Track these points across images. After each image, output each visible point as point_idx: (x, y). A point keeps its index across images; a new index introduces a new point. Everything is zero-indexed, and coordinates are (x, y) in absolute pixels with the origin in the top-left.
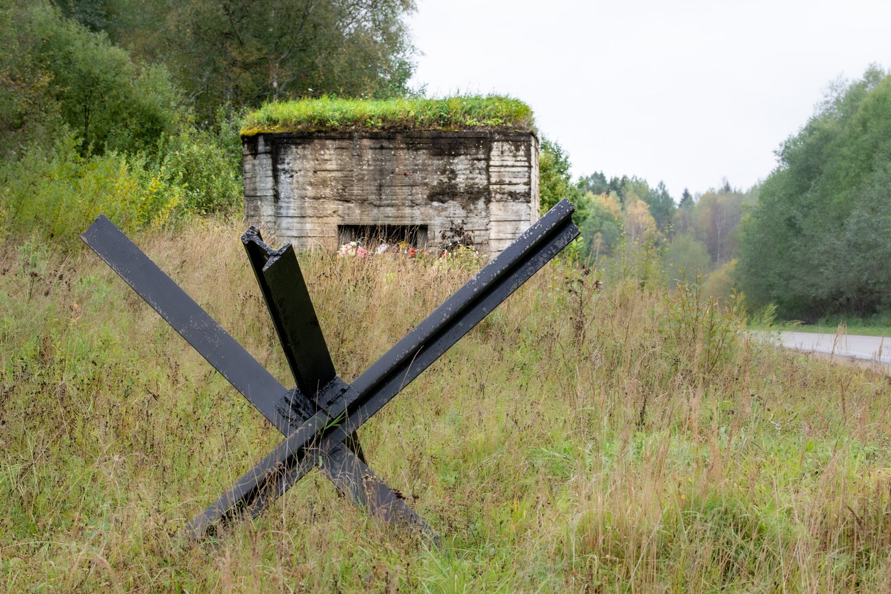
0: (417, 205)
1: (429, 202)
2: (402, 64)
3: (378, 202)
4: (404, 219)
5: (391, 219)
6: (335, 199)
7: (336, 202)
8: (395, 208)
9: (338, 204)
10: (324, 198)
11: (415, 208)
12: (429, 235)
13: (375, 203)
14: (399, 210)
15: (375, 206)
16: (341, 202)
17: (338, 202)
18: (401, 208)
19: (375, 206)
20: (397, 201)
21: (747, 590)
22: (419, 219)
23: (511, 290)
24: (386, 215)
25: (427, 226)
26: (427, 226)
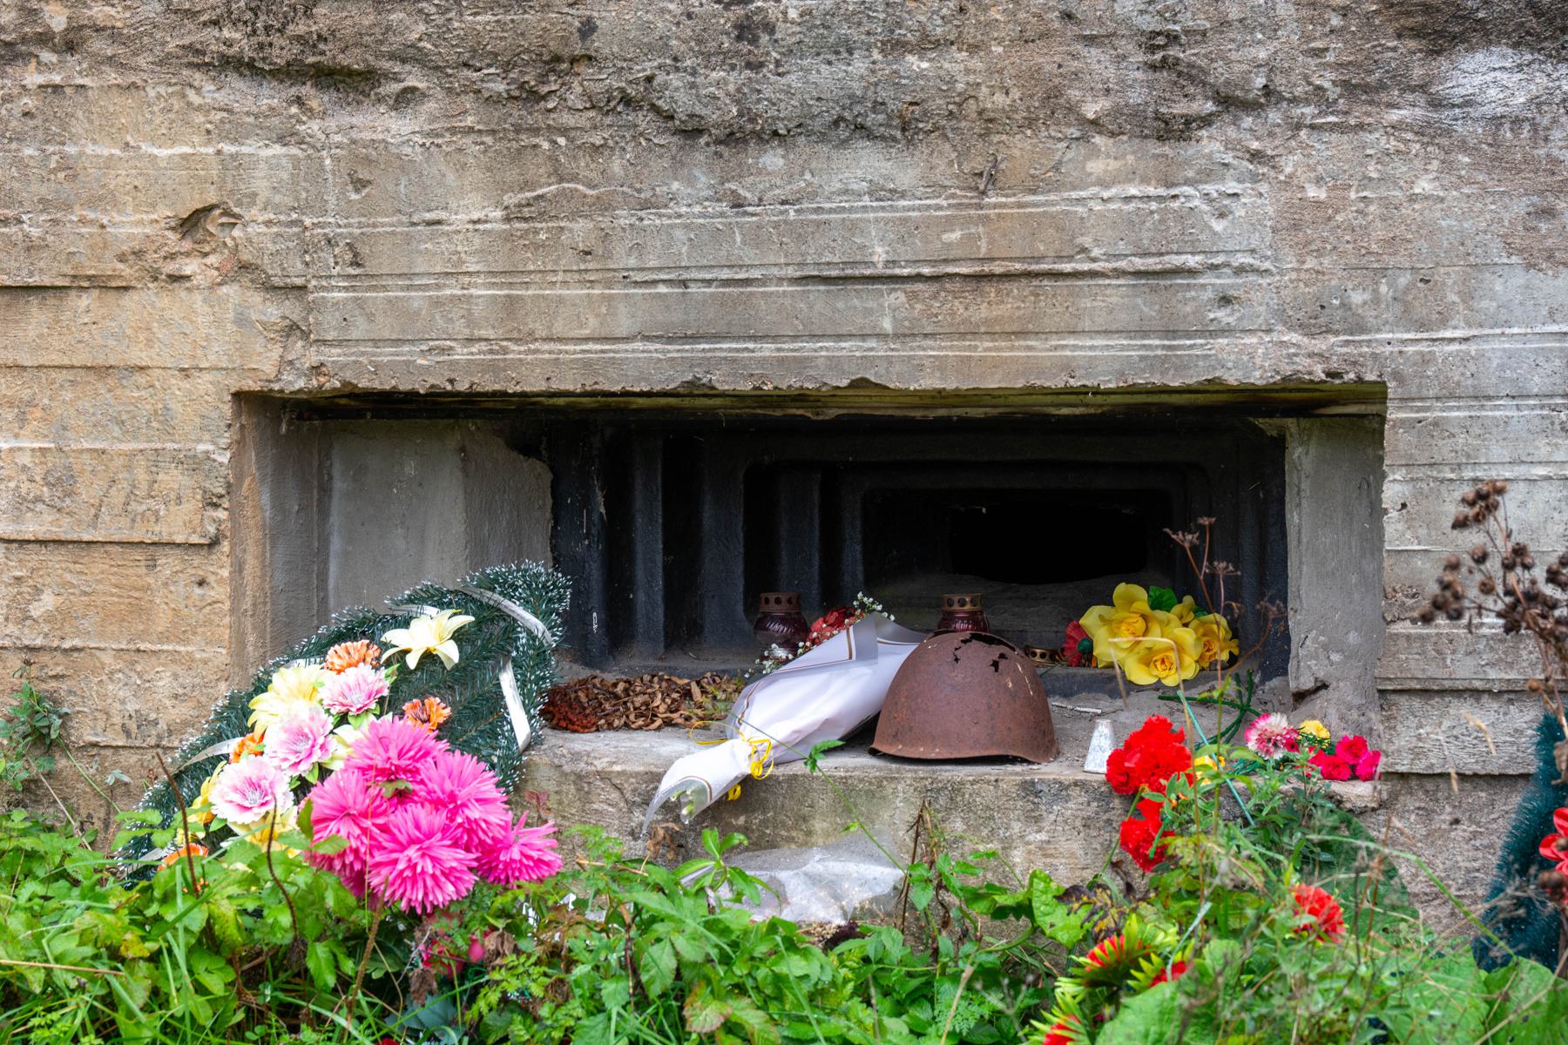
0: (1231, 102)
1: (1397, 50)
2: (1498, 503)
3: (723, 81)
4: (1052, 303)
5: (890, 307)
6: (194, 58)
7: (208, 91)
8: (941, 160)
9: (231, 127)
10: (70, 44)
11: (1210, 144)
12: (1395, 531)
13: (678, 93)
14: (989, 179)
15: (692, 132)
16: (270, 97)
17: (241, 94)
18: (1019, 148)
19: (692, 132)
20: (956, 63)
21: (981, 175)
22: (1261, 298)
23: (728, 402)
24: (830, 255)
25: (1376, 394)
26: (1376, 394)
